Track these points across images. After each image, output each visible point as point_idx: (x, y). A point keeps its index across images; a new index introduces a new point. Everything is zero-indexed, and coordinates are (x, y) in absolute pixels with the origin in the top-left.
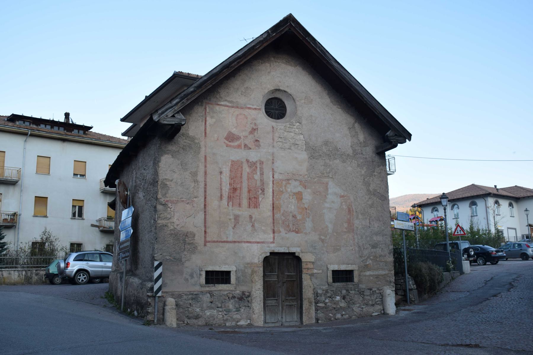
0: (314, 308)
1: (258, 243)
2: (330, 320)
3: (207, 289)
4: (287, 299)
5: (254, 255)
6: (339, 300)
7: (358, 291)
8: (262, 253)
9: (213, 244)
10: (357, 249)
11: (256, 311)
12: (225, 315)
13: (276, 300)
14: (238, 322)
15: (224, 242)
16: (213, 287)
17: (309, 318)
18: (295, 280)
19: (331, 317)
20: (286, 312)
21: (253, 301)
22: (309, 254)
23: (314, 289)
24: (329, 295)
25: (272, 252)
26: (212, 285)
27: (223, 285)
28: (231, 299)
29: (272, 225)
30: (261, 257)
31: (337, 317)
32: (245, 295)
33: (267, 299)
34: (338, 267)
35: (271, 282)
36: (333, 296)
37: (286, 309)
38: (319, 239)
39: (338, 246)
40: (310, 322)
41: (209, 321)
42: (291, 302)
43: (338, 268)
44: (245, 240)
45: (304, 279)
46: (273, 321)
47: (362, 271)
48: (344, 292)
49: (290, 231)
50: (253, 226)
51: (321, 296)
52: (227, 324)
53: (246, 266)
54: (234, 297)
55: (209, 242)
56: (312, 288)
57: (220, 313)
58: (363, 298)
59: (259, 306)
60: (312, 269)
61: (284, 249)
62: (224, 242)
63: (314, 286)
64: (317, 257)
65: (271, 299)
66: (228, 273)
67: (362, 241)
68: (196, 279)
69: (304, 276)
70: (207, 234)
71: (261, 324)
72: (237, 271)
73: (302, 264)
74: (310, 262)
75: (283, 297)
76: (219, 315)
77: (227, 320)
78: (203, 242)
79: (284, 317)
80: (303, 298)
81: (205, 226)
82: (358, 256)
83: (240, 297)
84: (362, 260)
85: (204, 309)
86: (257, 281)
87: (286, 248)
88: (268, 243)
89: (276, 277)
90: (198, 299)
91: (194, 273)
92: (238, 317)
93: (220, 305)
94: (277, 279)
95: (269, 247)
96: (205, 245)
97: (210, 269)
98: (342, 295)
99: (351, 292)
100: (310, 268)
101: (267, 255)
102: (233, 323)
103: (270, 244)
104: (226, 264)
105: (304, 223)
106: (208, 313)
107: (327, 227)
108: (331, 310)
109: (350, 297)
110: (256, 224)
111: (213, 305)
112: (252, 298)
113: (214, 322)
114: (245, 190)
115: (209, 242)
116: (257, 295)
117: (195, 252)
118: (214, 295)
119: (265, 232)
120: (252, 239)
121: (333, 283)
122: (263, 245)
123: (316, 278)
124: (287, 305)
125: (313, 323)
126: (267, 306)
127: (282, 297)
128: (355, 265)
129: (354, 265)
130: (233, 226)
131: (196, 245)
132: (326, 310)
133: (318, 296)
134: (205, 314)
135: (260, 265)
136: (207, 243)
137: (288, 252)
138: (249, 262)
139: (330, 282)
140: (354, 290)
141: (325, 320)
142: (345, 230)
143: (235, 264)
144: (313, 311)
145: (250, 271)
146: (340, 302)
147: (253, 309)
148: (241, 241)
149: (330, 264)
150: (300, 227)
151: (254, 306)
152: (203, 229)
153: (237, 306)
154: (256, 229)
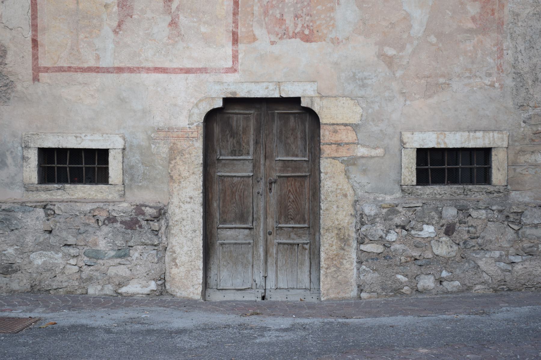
0: (354, 256)
1: (188, 71)
2: (397, 291)
3: (44, 196)
4: (281, 228)
5: (175, 105)
6: (433, 235)
7: (500, 211)
8: (201, 101)
9: (59, 75)
10: (509, 82)
11: (182, 258)
12: (85, 267)
13: (250, 229)
14: (120, 285)
15: (90, 70)
16: (60, 192)
17: (339, 283)
18: (306, 176)
19: (401, 283)
20: (276, 263)
21: (172, 232)
22: (343, 100)
23: (356, 201)
24: (398, 220)
25: (230, 96)
26: (56, 186)
27: (88, 186)
28: (104, 223)
29: (230, 19)
30: (196, 111)
31: (420, 286)
32: (143, 214)
33: (221, 226)
34: (438, 138)
35: (235, 180)
36: (413, 223)
37: (277, 253)
38: (378, 57)
39: (443, 76)
40: (342, 295)
41: (40, 282)
42: (293, 235)
43: (438, 143)
44: (150, 65)
45: (326, 173)
46: (238, 283)
47: (522, 151)
48: (450, 213)
49: (285, 35)
50: (173, 24)
51: (373, 222)
52: (91, 291)
53: (153, 135)
54: (111, 220)
55: (47, 70)
56: (351, 198)
57: (73, 261)
58: (517, 232)
59: (189, 243)
60: (352, 146)
61: (267, 88)
62: (90, 70)
63: (355, 194)
64: (370, 111)
65: (234, 226)
66: (103, 154)
67: (530, 58)
68: (12, 169)
69: (325, 164)
70: (40, 49)
71: (196, 292)
72: (128, 149)
73: (322, 132)
74: (346, 125)
75: (271, 222)
76: (68, 266)
77: (90, 279)
78: (30, 71)
79: (271, 275)
80: (322, 226)
81: (34, 27)
82: (510, 104)
83: (128, 219)
84: (525, 115)
85: (26, 250)
86: (185, 178)
87: (272, 86)
88: (217, 71)
89: (250, 166)
90: (12, 224)
91: (8, 153)
92: (120, 273)
93: (71, 240)
94: (253, 172)
95: (220, 83)
96: (36, 79)
97: (51, 143)
98: (443, 221)
99: (474, 214)
100: (346, 141)
101: (216, 106)
102: (106, 288)
103: (224, 75)
104: (94, 130)
105: (332, 9)
106: (38, 259)
107: (407, 17)
108: (401, 265)
109: (471, 229)
110: (181, 17)
111: (53, 240)
112: (170, 224)
113: (55, 285)
115: (47, 70)
116: (185, 216)
117: (9, 99)
118: (57, 212)
119: (207, 40)
120: (171, 61)
121: (419, 187)
122: (203, 76)
123: (365, 171)
124: (279, 244)
125: (352, 298)
126: (222, 244)
127: (265, 223)
128: (500, 131)
129: (496, 134)
130: (115, 24)
131: (12, 78)
132: (386, 263)
133: (363, 224)
134: (30, 262)
135: (195, 134)
136: (40, 74)
137: (277, 95)
138: (161, 125)
139: (409, 183)
140: (486, 208)
141: (379, 291)
142: (471, 25)
143: (122, 131)
144: (352, 264)
145: (164, 150)
146: (432, 242)
147: (174, 252)
148: (138, 68)
149: (412, 130)
150: (318, 23)
151: (174, 243)
152: (29, 35)
153: (119, 242)
154: (183, 32)
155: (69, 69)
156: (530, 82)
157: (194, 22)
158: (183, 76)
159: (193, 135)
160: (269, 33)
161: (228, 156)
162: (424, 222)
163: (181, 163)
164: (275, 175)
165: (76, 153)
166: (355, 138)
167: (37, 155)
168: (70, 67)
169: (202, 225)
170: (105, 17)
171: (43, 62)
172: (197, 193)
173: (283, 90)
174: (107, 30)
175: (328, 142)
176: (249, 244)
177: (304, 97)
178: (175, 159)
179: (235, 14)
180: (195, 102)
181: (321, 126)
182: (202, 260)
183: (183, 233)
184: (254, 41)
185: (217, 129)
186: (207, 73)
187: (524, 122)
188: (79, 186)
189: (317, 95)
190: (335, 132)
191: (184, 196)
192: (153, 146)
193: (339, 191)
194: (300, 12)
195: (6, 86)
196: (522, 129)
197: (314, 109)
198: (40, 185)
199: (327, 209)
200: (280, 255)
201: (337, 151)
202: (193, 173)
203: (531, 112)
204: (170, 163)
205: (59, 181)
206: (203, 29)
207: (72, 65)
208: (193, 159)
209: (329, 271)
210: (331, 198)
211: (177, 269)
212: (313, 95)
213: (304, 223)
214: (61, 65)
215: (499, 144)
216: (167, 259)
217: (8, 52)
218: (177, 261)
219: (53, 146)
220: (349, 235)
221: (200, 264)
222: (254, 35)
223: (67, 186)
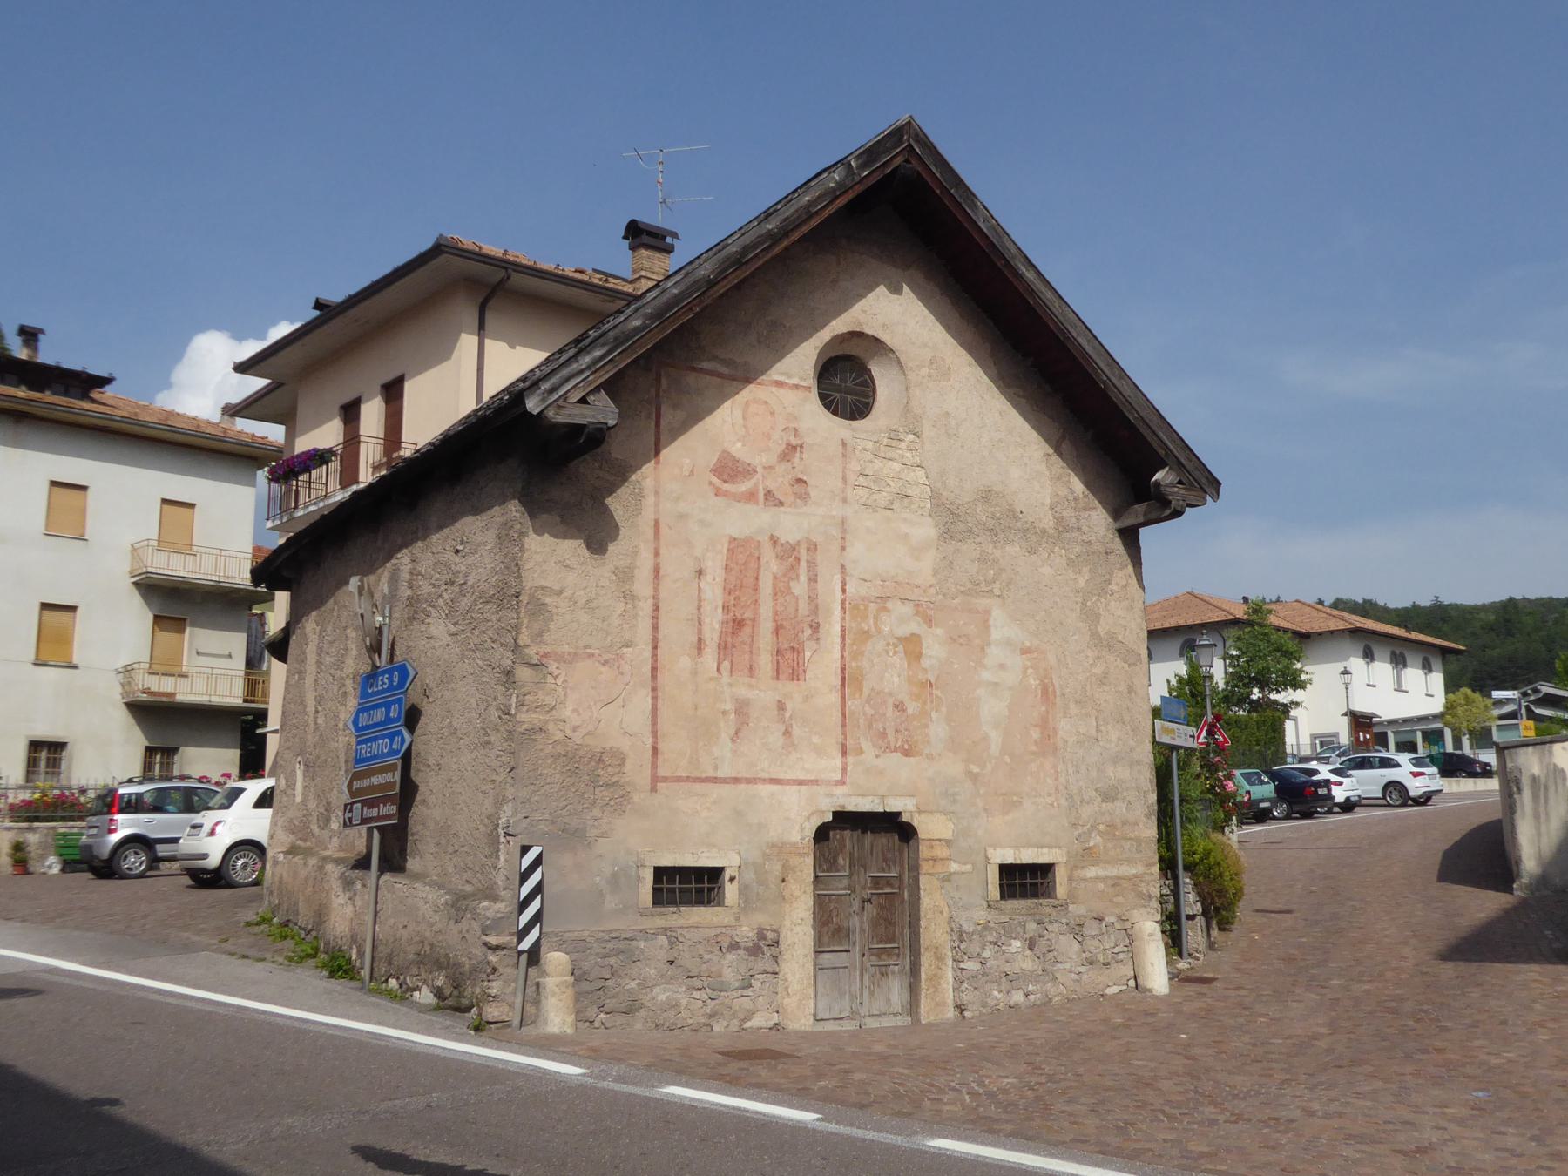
1: (800, 783)
3: (660, 922)
6: (1019, 950)
11: (794, 986)
16: (675, 916)
25: (839, 809)
29: (840, 729)
30: (807, 824)
44: (766, 776)
50: (787, 733)
55: (665, 779)
74: (940, 840)
81: (655, 733)
84: (1076, 833)
86: (797, 898)
88: (828, 783)
96: (654, 789)
97: (667, 861)
98: (1026, 936)
100: (941, 856)
101: (826, 821)
105: (927, 726)
110: (794, 727)
115: (665, 779)
116: (796, 940)
119: (819, 751)
129: (1057, 851)
130: (733, 732)
135: (806, 850)
137: (882, 810)
139: (994, 898)
142: (1034, 748)
148: (755, 779)
149: (994, 846)
152: (649, 742)
154: (796, 742)
155: (688, 779)
158: (795, 788)
162: (1011, 937)
170: (722, 724)
171: (662, 772)
206: (815, 740)
210: (930, 915)
214: (679, 774)
215: (1060, 859)
216: (780, 989)
222: (861, 748)
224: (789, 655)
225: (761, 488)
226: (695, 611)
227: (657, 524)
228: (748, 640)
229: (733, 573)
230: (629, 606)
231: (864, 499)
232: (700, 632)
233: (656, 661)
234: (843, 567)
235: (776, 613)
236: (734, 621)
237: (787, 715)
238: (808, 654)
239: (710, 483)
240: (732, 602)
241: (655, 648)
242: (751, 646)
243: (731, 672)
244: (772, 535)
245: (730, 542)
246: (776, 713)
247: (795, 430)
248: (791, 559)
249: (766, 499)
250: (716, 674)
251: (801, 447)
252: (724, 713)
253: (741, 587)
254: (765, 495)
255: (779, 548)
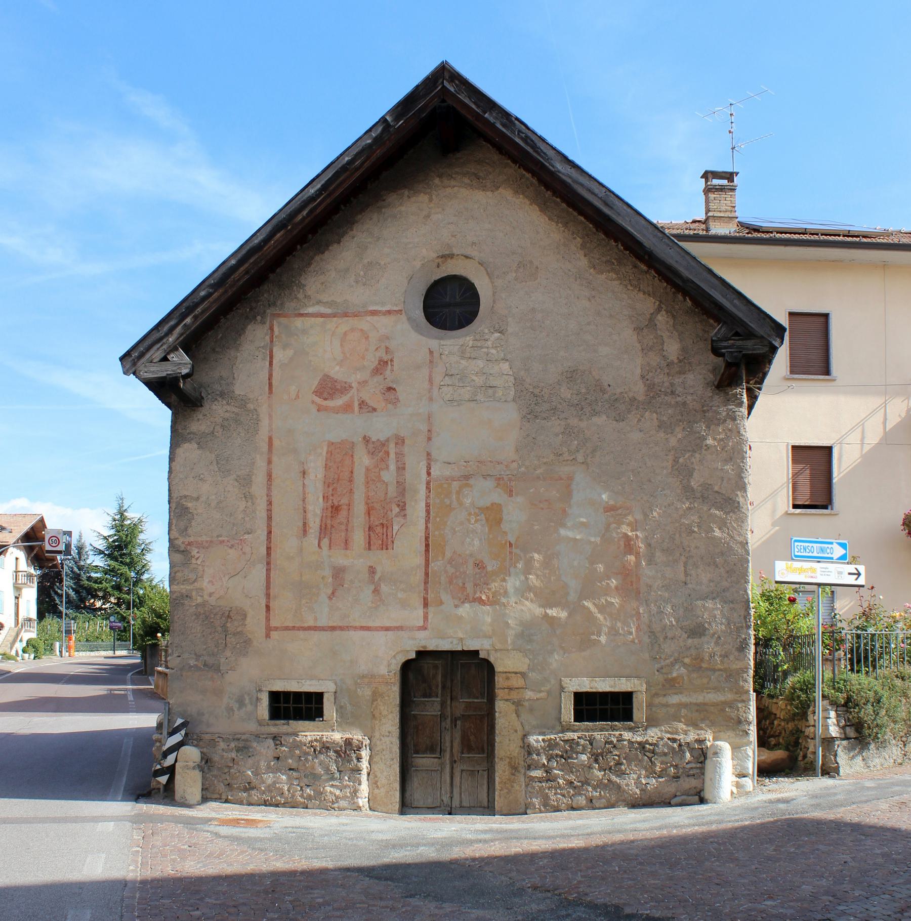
1: (387, 629)
8: (397, 653)
9: (286, 632)
10: (646, 640)
13: (439, 758)
15: (309, 628)
16: (286, 727)
25: (421, 649)
26: (282, 721)
30: (394, 661)
44: (357, 624)
47: (656, 695)
50: (376, 591)
55: (276, 629)
61: (452, 643)
62: (309, 628)
66: (319, 696)
69: (500, 706)
72: (338, 692)
74: (516, 673)
78: (264, 630)
81: (268, 596)
82: (646, 656)
84: (657, 666)
88: (411, 629)
96: (268, 636)
97: (279, 687)
101: (410, 658)
103: (417, 632)
110: (382, 585)
114: (359, 508)
115: (276, 629)
117: (247, 652)
118: (283, 742)
119: (404, 604)
122: (400, 633)
130: (330, 591)
135: (393, 680)
137: (460, 649)
138: (366, 672)
145: (368, 692)
147: (376, 776)
148: (347, 627)
152: (263, 602)
156: (662, 640)
157: (393, 590)
159: (391, 681)
160: (453, 598)
161: (420, 698)
163: (382, 704)
164: (458, 713)
165: (298, 696)
166: (524, 683)
167: (268, 696)
168: (294, 627)
169: (398, 754)
172: (395, 728)
173: (465, 644)
174: (323, 598)
175: (501, 686)
176: (438, 770)
177: (482, 650)
178: (377, 700)
179: (426, 583)
180: (393, 654)
181: (496, 674)
182: (398, 783)
183: (383, 760)
184: (441, 605)
185: (411, 676)
186: (402, 630)
187: (658, 671)
188: (301, 722)
189: (492, 648)
190: (508, 678)
191: (383, 730)
192: (359, 690)
193: (510, 727)
194: (478, 582)
195: (245, 642)
196: (656, 677)
197: (490, 660)
198: (270, 721)
199: (500, 742)
200: (325, 298)
201: (509, 694)
202: (391, 712)
203: (663, 664)
204: (372, 704)
205: (284, 719)
206: (400, 595)
207: (296, 625)
208: (391, 700)
209: (502, 792)
211: (378, 790)
212: (489, 648)
213: (483, 753)
217: (248, 615)
218: (378, 783)
219: (280, 690)
220: (518, 764)
221: (397, 786)
222: (441, 600)
223: (291, 722)
224: (379, 530)
225: (356, 399)
226: (301, 503)
227: (270, 439)
228: (345, 521)
229: (332, 469)
230: (250, 503)
231: (449, 396)
232: (305, 518)
233: (270, 542)
234: (428, 454)
235: (368, 498)
236: (332, 507)
237: (377, 577)
238: (396, 528)
239: (313, 402)
240: (330, 493)
241: (270, 533)
242: (347, 525)
243: (330, 546)
244: (365, 436)
245: (328, 446)
246: (367, 575)
247: (387, 348)
248: (381, 453)
249: (361, 408)
250: (317, 549)
251: (392, 360)
252: (323, 578)
253: (338, 480)
254: (360, 404)
255: (371, 446)
